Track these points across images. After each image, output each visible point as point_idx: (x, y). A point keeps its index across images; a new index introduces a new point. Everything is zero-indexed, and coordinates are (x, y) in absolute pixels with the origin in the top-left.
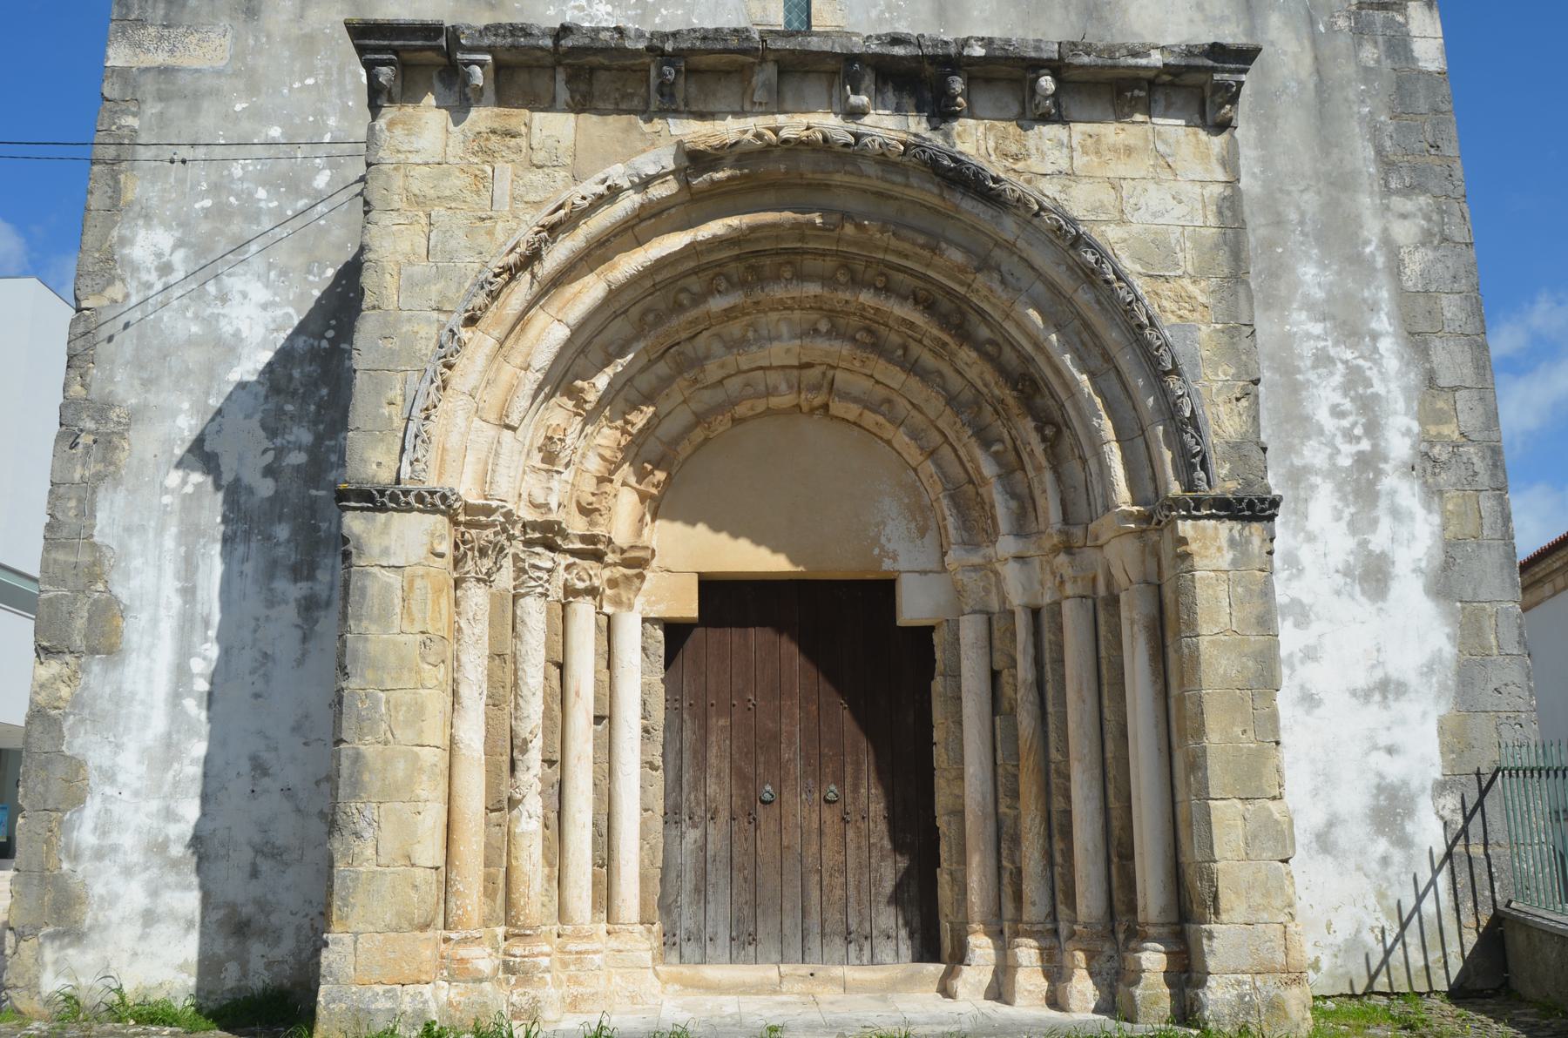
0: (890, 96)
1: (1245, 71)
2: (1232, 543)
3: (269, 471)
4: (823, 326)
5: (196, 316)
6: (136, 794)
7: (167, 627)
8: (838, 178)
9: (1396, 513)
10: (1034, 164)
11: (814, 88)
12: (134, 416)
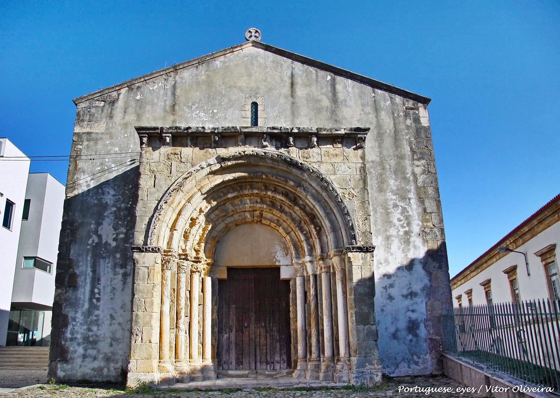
0: (274, 142)
1: (367, 134)
2: (362, 258)
3: (115, 240)
4: (259, 200)
5: (96, 198)
6: (81, 324)
7: (88, 281)
8: (261, 163)
9: (415, 247)
10: (311, 160)
11: (254, 141)
12: (82, 224)
